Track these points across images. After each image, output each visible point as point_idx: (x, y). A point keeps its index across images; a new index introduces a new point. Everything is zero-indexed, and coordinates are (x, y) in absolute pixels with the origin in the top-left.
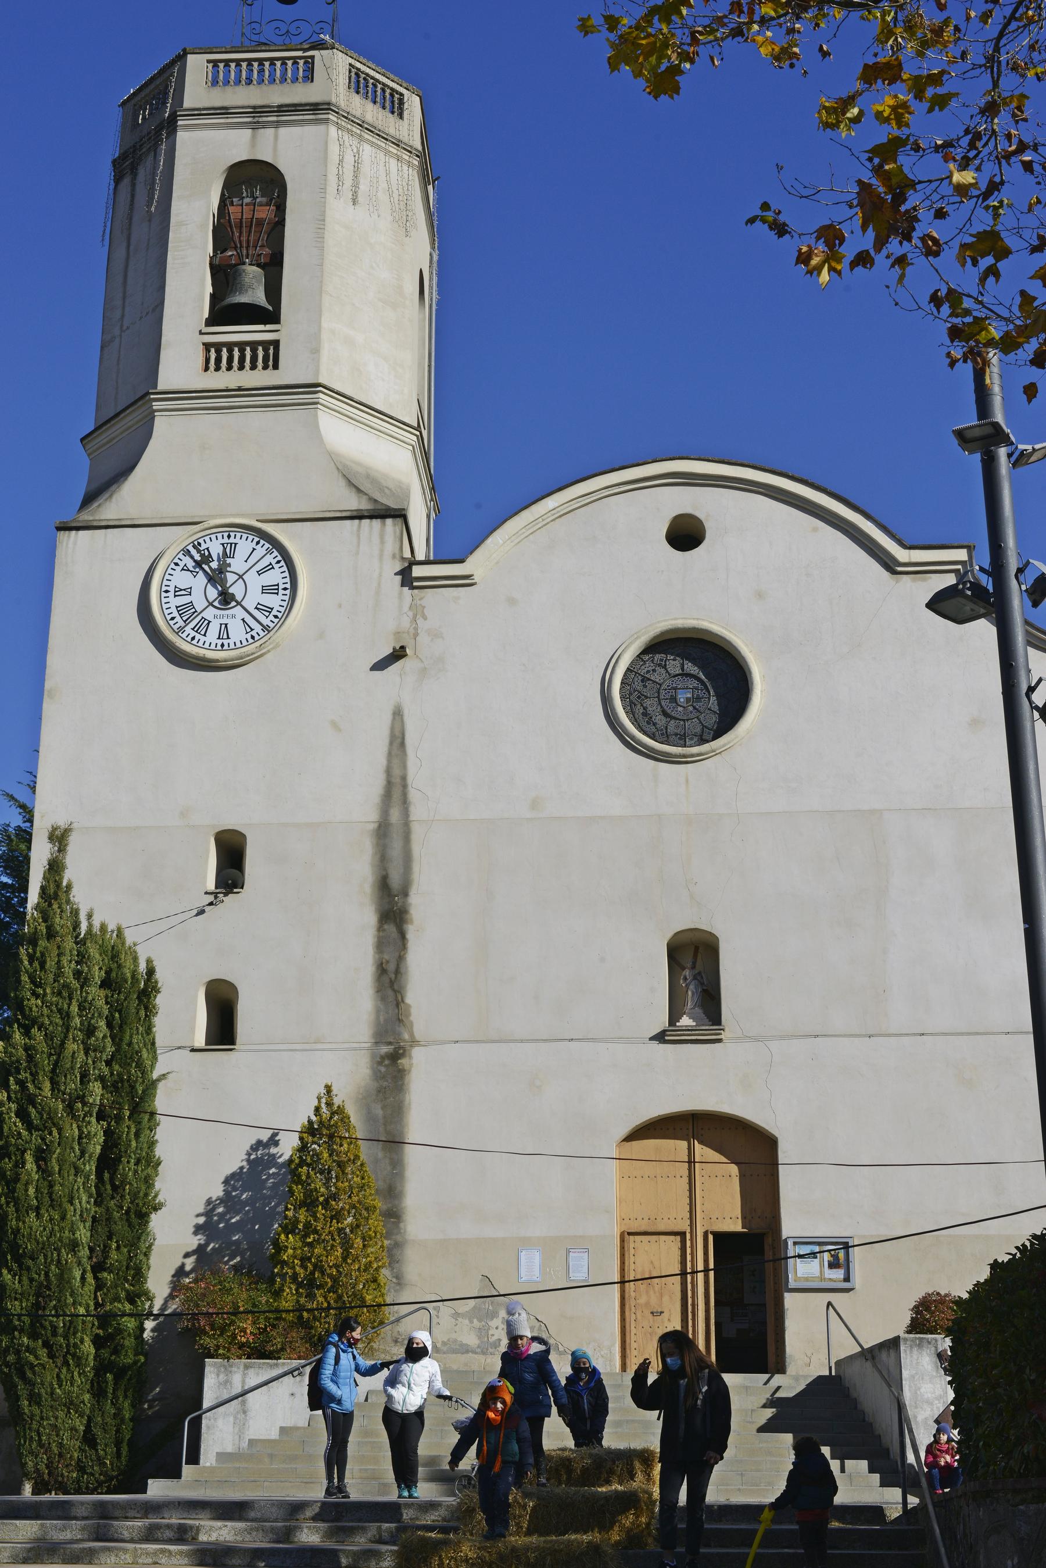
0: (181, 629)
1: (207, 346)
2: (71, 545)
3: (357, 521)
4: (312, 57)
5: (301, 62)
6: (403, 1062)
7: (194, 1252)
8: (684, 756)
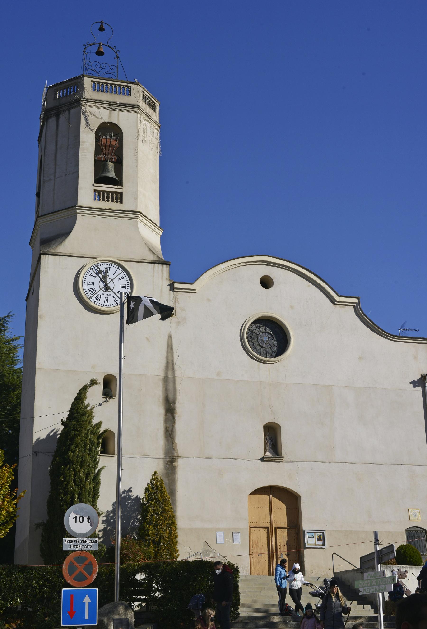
0: (91, 298)
1: (95, 191)
2: (46, 261)
3: (153, 264)
4: (131, 87)
5: (126, 87)
6: (175, 464)
7: (102, 530)
8: (269, 361)
